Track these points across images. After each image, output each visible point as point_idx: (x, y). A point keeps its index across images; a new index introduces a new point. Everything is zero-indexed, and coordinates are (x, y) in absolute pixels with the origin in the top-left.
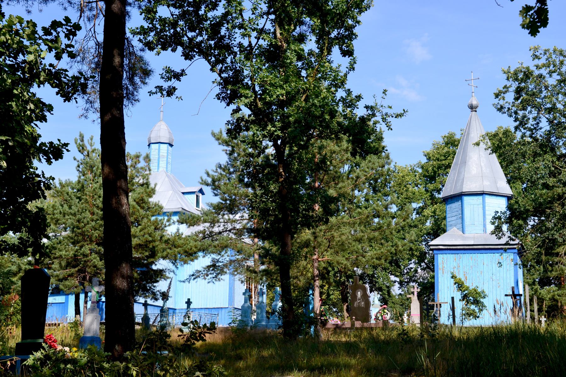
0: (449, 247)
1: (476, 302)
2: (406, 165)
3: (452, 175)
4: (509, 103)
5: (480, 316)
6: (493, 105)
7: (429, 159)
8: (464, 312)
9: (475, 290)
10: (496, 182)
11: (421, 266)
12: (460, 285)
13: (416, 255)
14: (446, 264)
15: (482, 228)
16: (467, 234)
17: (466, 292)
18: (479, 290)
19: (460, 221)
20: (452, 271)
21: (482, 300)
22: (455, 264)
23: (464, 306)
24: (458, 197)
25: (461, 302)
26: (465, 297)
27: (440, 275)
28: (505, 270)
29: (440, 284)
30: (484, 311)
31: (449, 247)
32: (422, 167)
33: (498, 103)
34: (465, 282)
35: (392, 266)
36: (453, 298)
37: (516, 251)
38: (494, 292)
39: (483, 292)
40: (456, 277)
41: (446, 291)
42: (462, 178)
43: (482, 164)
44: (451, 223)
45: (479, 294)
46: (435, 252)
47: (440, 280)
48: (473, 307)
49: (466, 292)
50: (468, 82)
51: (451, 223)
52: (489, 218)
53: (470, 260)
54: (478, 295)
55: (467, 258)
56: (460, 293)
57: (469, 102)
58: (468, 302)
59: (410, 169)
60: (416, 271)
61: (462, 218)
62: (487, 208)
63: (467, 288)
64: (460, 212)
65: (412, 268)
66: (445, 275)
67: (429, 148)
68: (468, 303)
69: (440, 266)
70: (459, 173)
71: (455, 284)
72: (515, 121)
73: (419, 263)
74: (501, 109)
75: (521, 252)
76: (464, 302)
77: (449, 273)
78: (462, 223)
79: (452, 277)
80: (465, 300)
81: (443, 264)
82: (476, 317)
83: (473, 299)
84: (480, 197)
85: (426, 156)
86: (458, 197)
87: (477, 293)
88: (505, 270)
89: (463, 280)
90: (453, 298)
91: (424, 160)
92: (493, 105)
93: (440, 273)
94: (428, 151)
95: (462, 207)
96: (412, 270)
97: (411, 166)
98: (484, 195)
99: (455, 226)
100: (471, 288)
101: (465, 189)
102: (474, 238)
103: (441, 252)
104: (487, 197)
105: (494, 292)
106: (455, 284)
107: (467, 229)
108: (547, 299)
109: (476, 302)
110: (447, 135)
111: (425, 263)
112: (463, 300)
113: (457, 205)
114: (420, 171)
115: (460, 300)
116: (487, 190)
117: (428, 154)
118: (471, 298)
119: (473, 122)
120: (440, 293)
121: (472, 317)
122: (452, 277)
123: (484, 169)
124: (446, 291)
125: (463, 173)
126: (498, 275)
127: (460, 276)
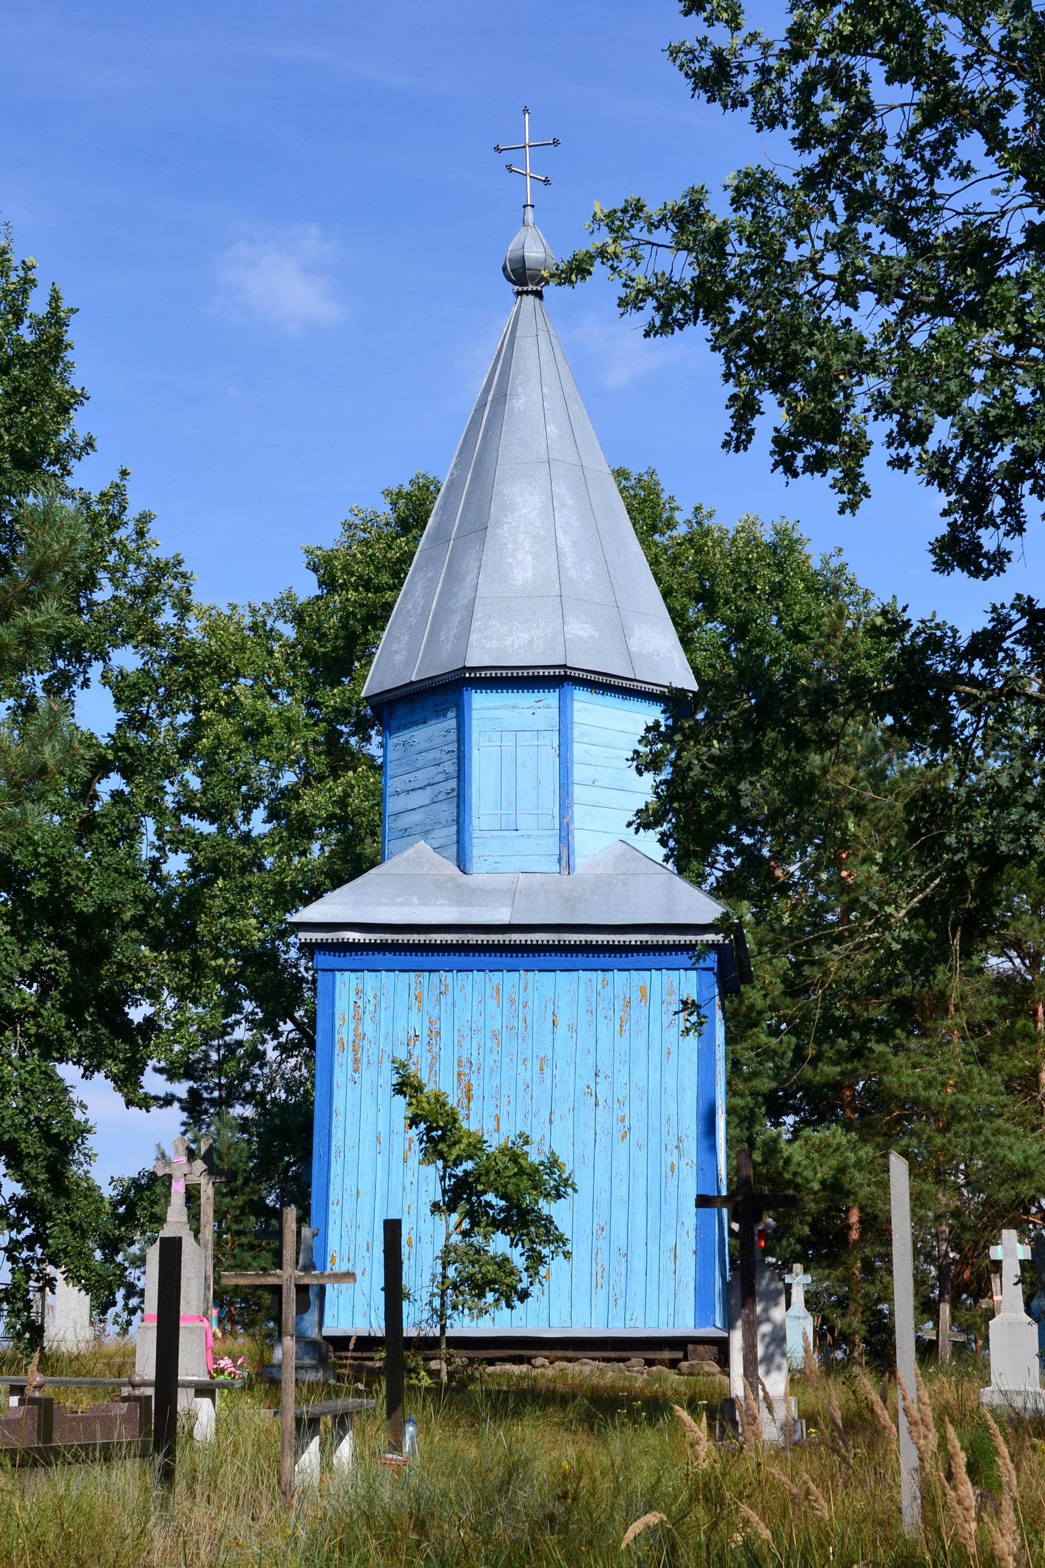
0: (389, 937)
1: (521, 1221)
2: (234, 607)
3: (419, 592)
4: (766, 46)
5: (535, 1290)
6: (674, 52)
7: (329, 583)
8: (451, 1272)
9: (515, 1158)
10: (623, 631)
11: (277, 1035)
12: (437, 1130)
13: (218, 971)
14: (371, 1017)
15: (552, 844)
16: (478, 877)
17: (469, 1165)
18: (534, 1156)
19: (447, 811)
20: (401, 1055)
21: (545, 1207)
22: (417, 1022)
23: (456, 1238)
24: (445, 693)
25: (440, 1221)
26: (458, 1195)
27: (339, 1077)
28: (655, 1053)
29: (337, 1121)
30: (556, 1267)
31: (389, 937)
32: (298, 618)
33: (703, 42)
34: (461, 1114)
35: (82, 1024)
36: (392, 1229)
37: (712, 960)
38: (602, 1163)
39: (553, 1163)
40: (419, 1089)
41: (366, 1155)
42: (463, 597)
43: (563, 541)
44: (405, 821)
45: (532, 1176)
46: (323, 960)
47: (338, 1102)
48: (499, 1244)
49: (469, 1165)
50: (506, 157)
51: (405, 821)
52: (965, 182)
53: (492, 1004)
54: (525, 1183)
55: (474, 995)
56: (432, 1172)
57: (512, 249)
58: (472, 1215)
59: (247, 621)
60: (257, 1056)
61: (460, 797)
62: (578, 750)
63: (476, 1147)
64: (450, 767)
65: (239, 1043)
66: (368, 1074)
67: (330, 538)
68: (475, 1223)
69: (344, 1032)
70: (453, 579)
71: (414, 1121)
72: (802, 144)
73: (268, 1025)
74: (714, 79)
75: (731, 970)
76: (455, 1217)
77: (387, 1065)
78: (461, 820)
79: (400, 1089)
80: (463, 1206)
81: (358, 1019)
82: (513, 1295)
83: (501, 1197)
84: (550, 698)
85: (315, 570)
86: (445, 693)
87: (521, 1172)
88: (655, 1053)
89: (452, 1101)
90: (392, 1229)
91: (307, 587)
92: (674, 52)
93: (343, 1061)
94: (328, 545)
95: (458, 807)
96: (241, 1051)
97: (254, 611)
98: (568, 687)
99: (425, 834)
100: (494, 1142)
101: (480, 654)
102: (512, 895)
103: (350, 960)
104: (583, 701)
105: (602, 1163)
106: (414, 1121)
107: (479, 849)
108: (816, 1186)
109: (521, 1221)
110: (407, 488)
111: (294, 1020)
112: (451, 1208)
113: (431, 735)
114: (288, 631)
115: (436, 1207)
116: (582, 660)
117: (328, 560)
118: (490, 1197)
119: (525, 344)
120: (336, 1169)
121: (490, 1297)
122: (400, 1089)
123: (569, 562)
124: (366, 1155)
125: (470, 579)
126: (622, 1078)
127: (441, 1081)
